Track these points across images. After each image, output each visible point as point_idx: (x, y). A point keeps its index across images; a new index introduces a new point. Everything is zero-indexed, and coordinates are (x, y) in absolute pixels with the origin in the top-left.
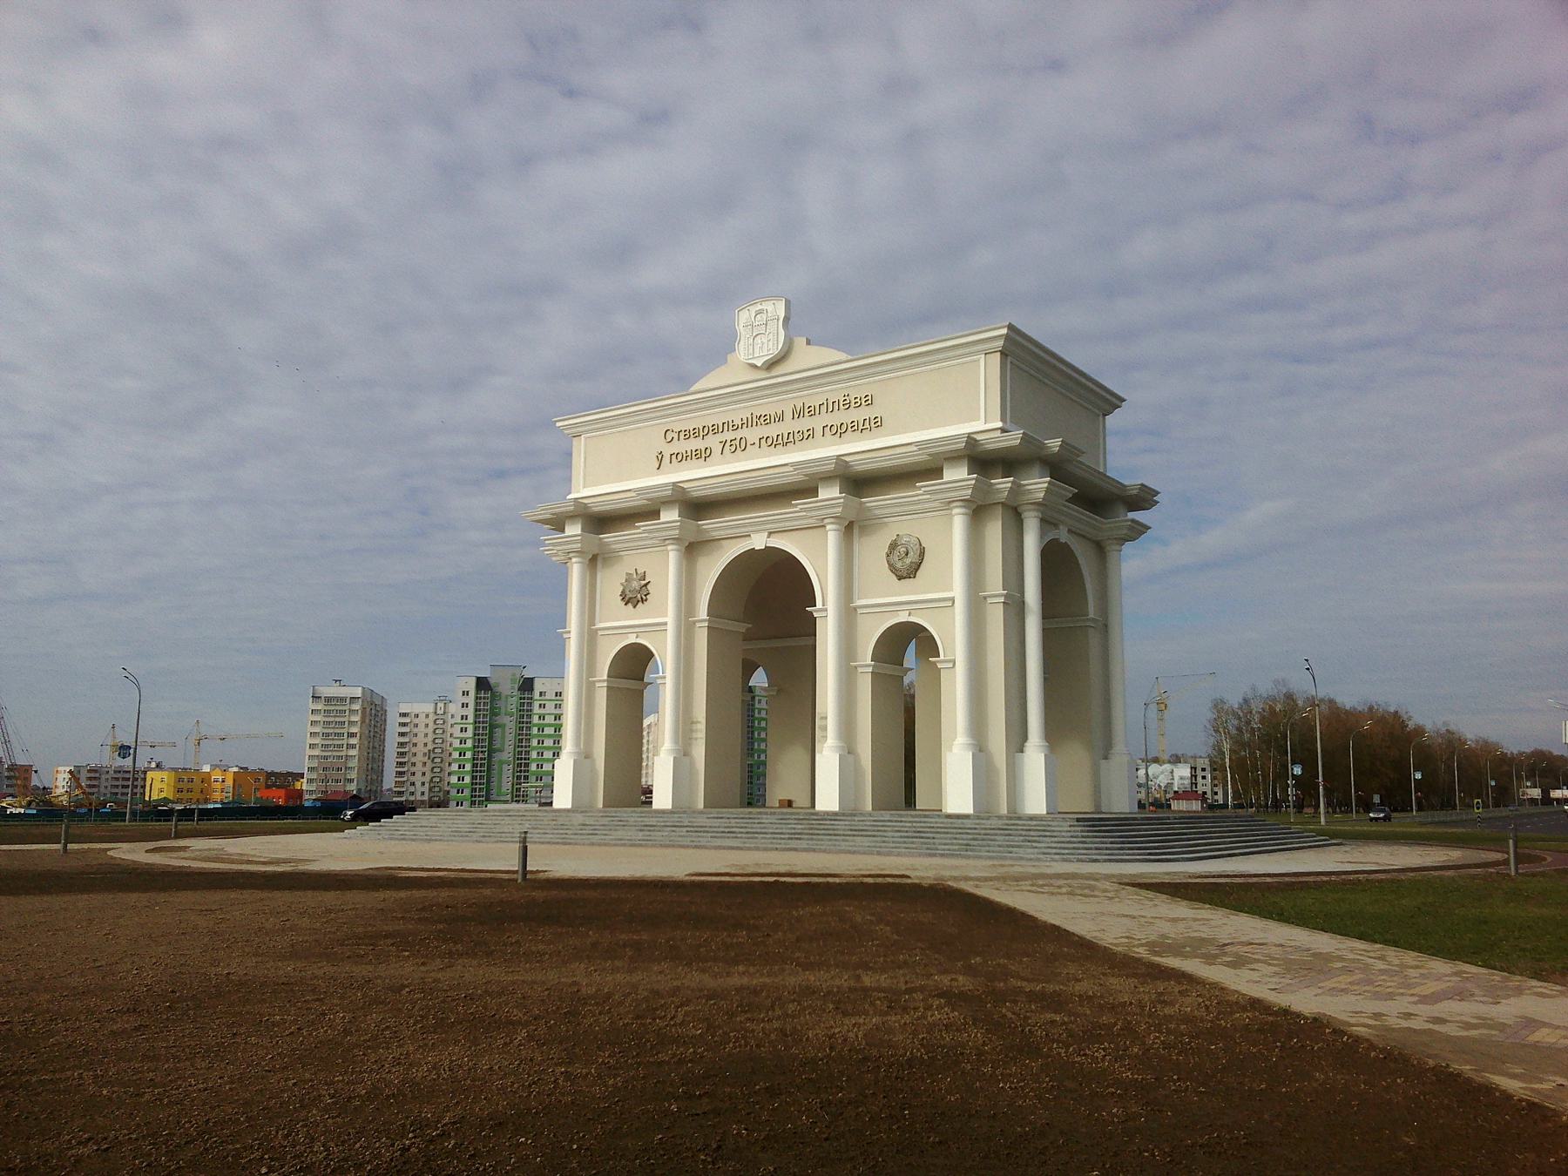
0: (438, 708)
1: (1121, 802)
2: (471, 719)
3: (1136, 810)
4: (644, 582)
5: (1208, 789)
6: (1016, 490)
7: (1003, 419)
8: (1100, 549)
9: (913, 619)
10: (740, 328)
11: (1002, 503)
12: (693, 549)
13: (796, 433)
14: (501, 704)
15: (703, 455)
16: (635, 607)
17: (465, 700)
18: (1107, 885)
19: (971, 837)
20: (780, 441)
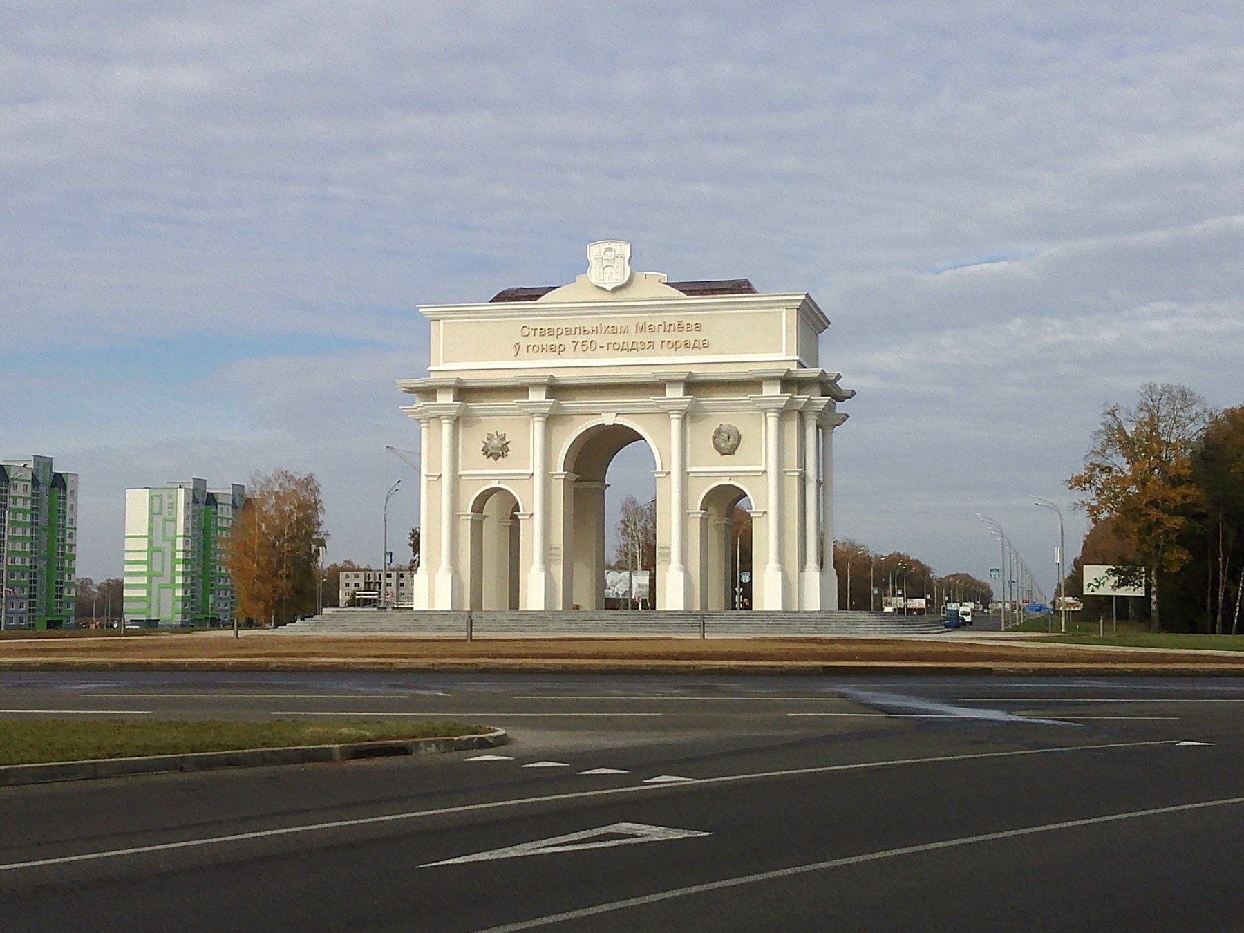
4: (504, 442)
10: (591, 258)
11: (798, 410)
12: (551, 420)
13: (639, 343)
15: (559, 350)
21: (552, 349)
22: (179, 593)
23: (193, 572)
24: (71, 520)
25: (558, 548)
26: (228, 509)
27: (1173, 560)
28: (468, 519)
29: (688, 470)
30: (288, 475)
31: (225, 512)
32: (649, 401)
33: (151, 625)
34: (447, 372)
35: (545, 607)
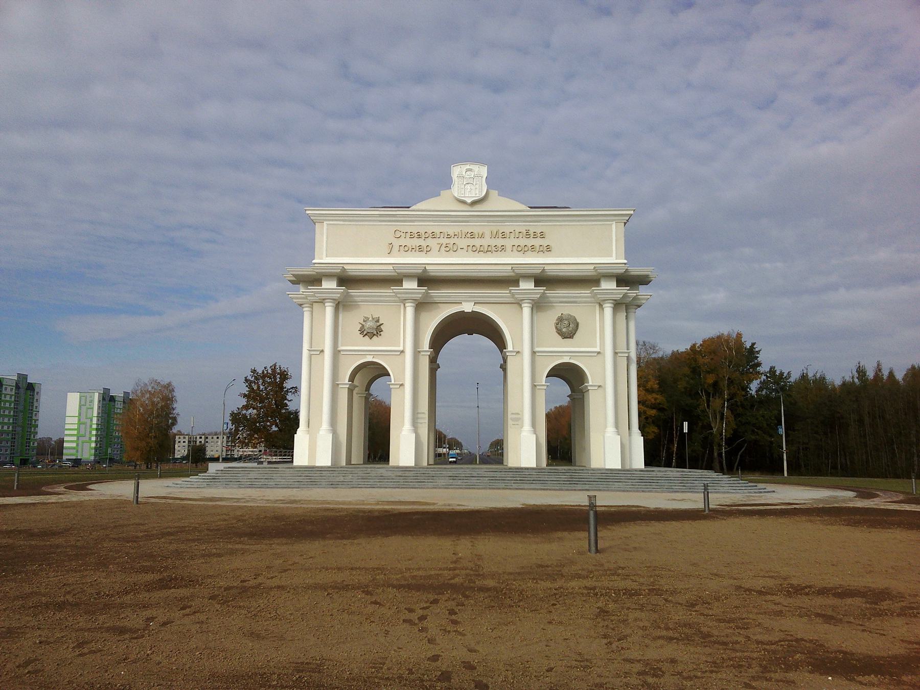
4: (378, 324)
9: (572, 361)
12: (421, 306)
15: (428, 251)
21: (420, 249)
22: (93, 445)
23: (101, 435)
24: (36, 407)
25: (423, 413)
26: (121, 404)
27: (651, 432)
30: (157, 381)
31: (119, 405)
33: (77, 462)
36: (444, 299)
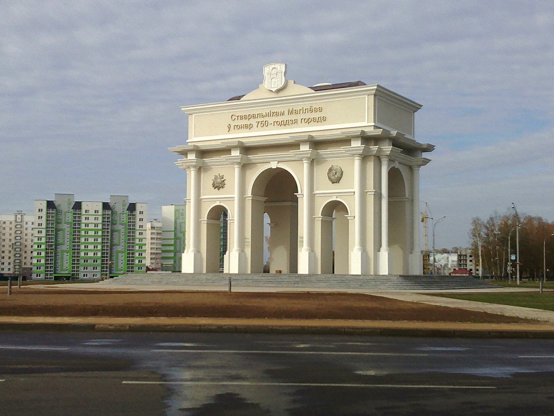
0: (18, 219)
1: (417, 270)
2: (44, 226)
3: (422, 274)
4: (223, 180)
5: (473, 267)
6: (380, 150)
7: (374, 122)
8: (411, 168)
9: (338, 199)
12: (245, 167)
13: (289, 121)
14: (62, 217)
15: (249, 127)
16: (219, 190)
17: (40, 214)
18: (409, 294)
19: (362, 282)
20: (283, 123)
21: (246, 127)
25: (248, 239)
28: (320, 220)
29: (202, 197)
32: (291, 153)
34: (255, 138)
35: (239, 272)
36: (259, 160)
